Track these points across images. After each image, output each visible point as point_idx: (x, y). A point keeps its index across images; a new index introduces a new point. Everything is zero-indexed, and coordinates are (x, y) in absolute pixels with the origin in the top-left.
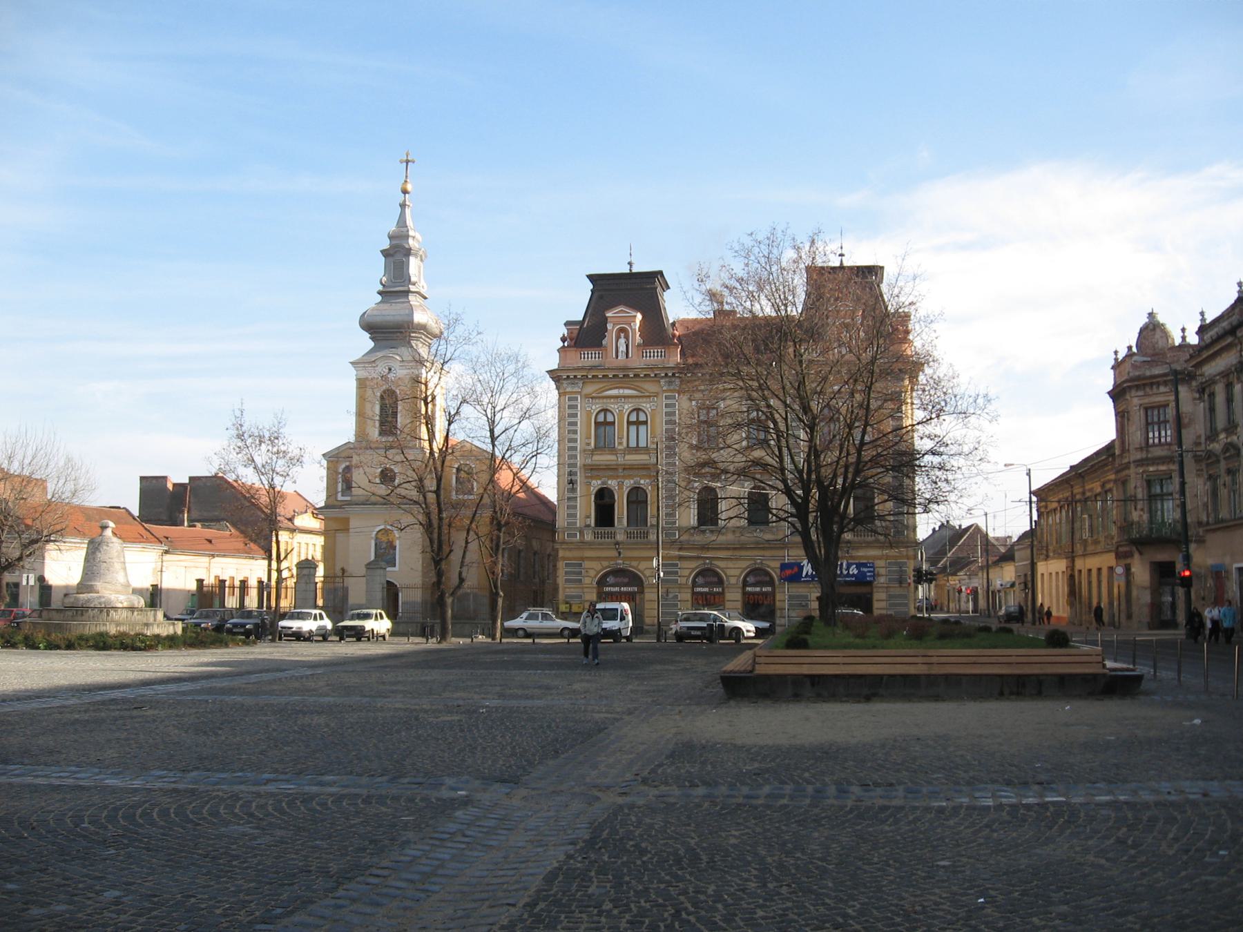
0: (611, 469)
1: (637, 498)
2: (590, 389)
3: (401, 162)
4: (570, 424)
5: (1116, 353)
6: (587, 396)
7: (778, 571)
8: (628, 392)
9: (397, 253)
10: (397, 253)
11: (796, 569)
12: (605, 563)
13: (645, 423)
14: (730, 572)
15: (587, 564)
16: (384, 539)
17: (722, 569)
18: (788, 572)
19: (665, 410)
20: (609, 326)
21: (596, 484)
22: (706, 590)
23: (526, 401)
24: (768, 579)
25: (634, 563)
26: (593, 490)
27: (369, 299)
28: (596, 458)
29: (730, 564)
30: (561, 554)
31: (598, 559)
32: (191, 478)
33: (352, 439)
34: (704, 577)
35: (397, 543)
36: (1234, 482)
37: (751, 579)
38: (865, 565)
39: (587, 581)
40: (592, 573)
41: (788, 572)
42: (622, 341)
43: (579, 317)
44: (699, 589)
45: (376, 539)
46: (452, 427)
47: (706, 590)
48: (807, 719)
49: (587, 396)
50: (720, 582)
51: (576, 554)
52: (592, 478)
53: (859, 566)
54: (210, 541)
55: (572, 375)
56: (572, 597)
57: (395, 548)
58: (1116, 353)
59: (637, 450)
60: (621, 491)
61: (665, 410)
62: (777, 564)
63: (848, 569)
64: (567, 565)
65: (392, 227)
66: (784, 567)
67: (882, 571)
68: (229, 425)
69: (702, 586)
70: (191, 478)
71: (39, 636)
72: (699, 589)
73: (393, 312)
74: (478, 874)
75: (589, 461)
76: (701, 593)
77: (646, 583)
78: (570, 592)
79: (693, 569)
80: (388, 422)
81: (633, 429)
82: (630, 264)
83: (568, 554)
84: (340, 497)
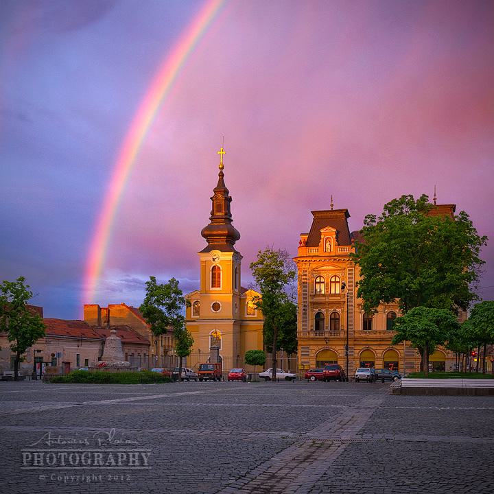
1: (335, 319)
4: (303, 291)
8: (331, 268)
9: (222, 175)
12: (320, 347)
13: (339, 282)
14: (377, 351)
15: (311, 347)
20: (322, 237)
21: (316, 310)
23: (307, 356)
25: (333, 347)
26: (315, 313)
29: (378, 348)
30: (299, 343)
36: (301, 379)
40: (314, 352)
42: (328, 244)
56: (304, 362)
59: (335, 295)
60: (327, 313)
74: (257, 483)
75: (312, 301)
78: (303, 360)
79: (361, 350)
81: (333, 285)
83: (302, 343)
84: (192, 317)
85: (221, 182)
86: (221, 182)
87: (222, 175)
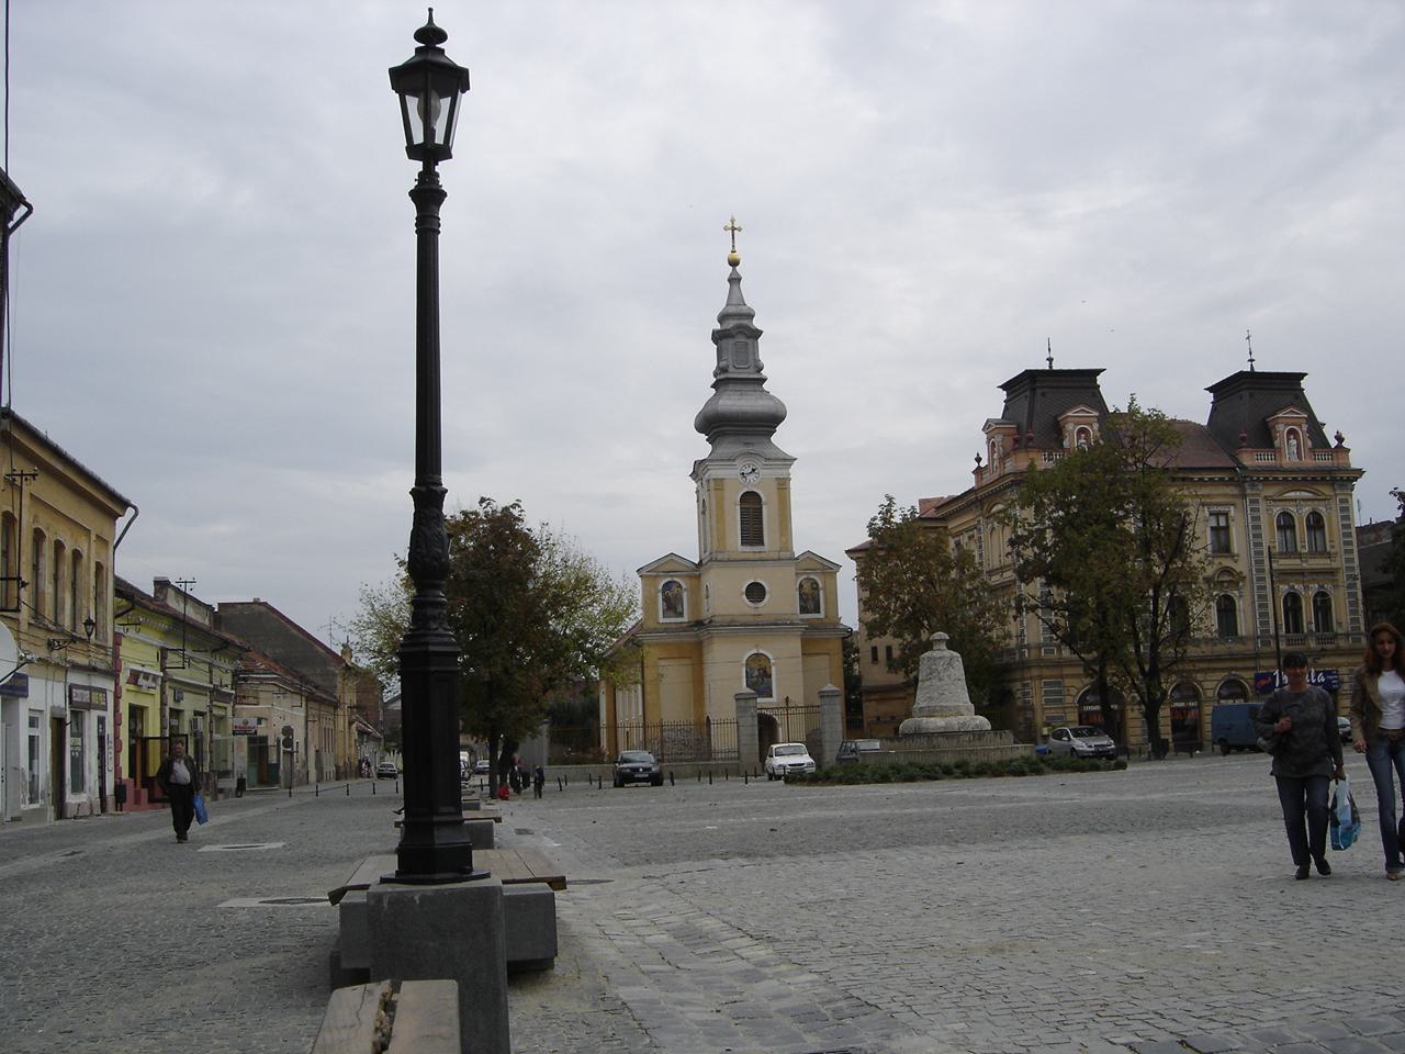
0: (1299, 573)
2: (1271, 491)
3: (726, 229)
5: (978, 460)
7: (1252, 682)
9: (736, 335)
10: (736, 335)
11: (1270, 679)
15: (1067, 682)
17: (1200, 683)
18: (1263, 682)
22: (1182, 704)
24: (1191, 693)
27: (700, 392)
34: (1179, 690)
37: (1225, 692)
38: (1330, 673)
39: (1069, 699)
40: (1073, 691)
41: (1263, 682)
43: (997, 413)
44: (1176, 704)
47: (1182, 704)
48: (821, 862)
50: (1196, 695)
51: (1056, 672)
53: (1326, 674)
56: (1053, 718)
57: (770, 676)
58: (978, 460)
62: (1250, 675)
63: (1316, 678)
66: (1258, 678)
67: (1346, 678)
68: (550, 528)
69: (1179, 701)
71: (1026, 769)
72: (1176, 704)
73: (735, 403)
76: (1178, 709)
77: (1203, 698)
78: (1049, 713)
82: (1050, 360)
84: (662, 620)
87: (735, 280)
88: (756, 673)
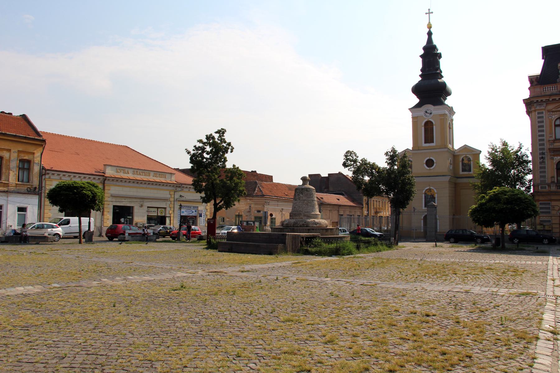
2: (550, 107)
6: (549, 111)
9: (430, 34)
15: (553, 203)
16: (429, 194)
19: (544, 129)
28: (555, 144)
31: (45, 201)
32: (329, 174)
33: (410, 147)
35: (436, 196)
39: (554, 212)
45: (425, 193)
46: (219, 214)
49: (549, 111)
52: (554, 155)
54: (339, 200)
55: (539, 100)
57: (434, 198)
61: (544, 129)
64: (541, 204)
65: (424, 43)
70: (329, 174)
75: (552, 147)
80: (429, 138)
85: (430, 40)
86: (430, 40)
87: (430, 34)
88: (429, 197)
